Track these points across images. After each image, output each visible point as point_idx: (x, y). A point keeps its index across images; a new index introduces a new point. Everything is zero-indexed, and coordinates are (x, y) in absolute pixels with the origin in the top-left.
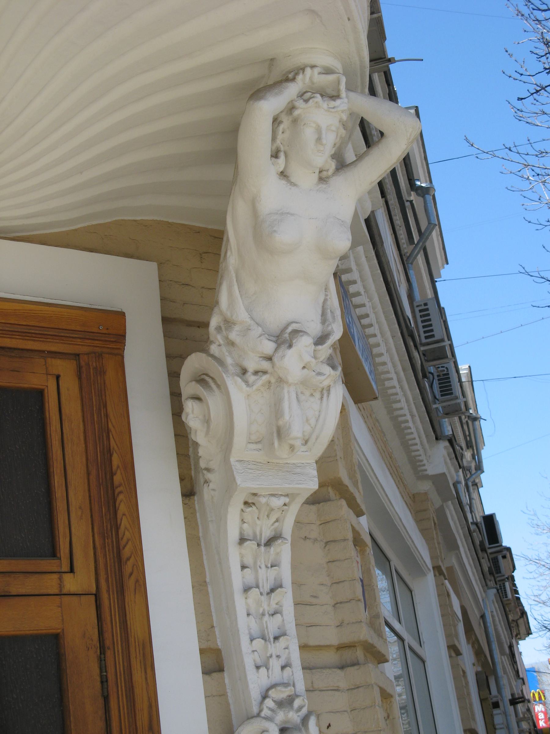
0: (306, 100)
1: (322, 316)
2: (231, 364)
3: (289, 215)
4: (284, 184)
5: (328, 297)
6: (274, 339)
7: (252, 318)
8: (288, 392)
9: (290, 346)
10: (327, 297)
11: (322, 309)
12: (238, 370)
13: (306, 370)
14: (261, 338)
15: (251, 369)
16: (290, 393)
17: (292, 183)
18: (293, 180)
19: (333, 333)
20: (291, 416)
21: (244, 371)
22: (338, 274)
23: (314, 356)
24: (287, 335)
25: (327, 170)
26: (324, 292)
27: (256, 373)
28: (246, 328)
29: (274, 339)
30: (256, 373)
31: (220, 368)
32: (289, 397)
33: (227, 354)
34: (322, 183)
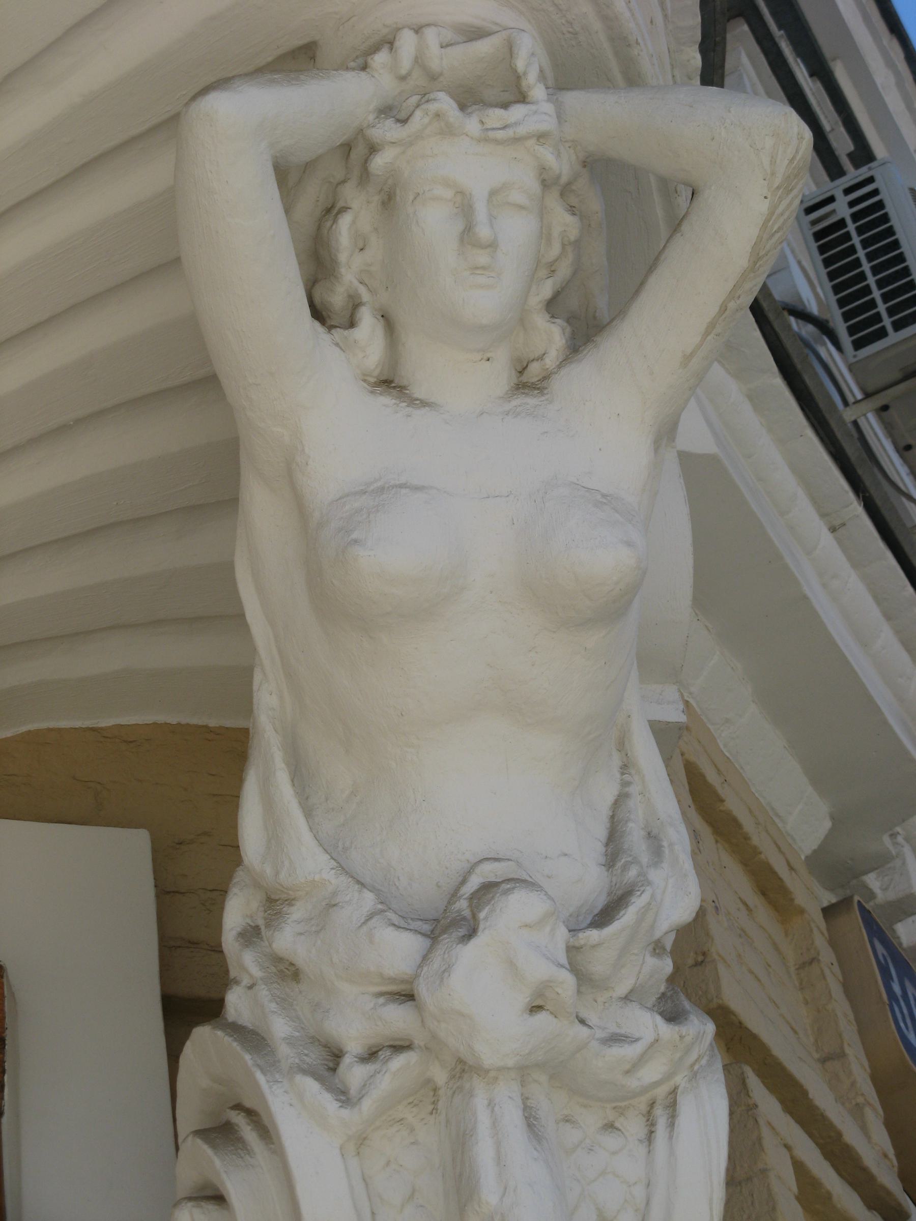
0: (405, 120)
1: (607, 845)
2: (284, 1039)
3: (404, 491)
4: (386, 406)
5: (632, 790)
6: (426, 928)
7: (343, 869)
8: (489, 1104)
9: (472, 933)
10: (627, 789)
11: (608, 825)
12: (314, 1057)
13: (542, 1018)
14: (373, 922)
15: (353, 1047)
16: (496, 1108)
17: (417, 400)
18: (419, 392)
19: (642, 889)
20: (506, 1188)
21: (335, 1055)
22: (856, 898)
23: (570, 964)
24: (462, 905)
25: (541, 358)
26: (618, 775)
27: (371, 1055)
28: (324, 904)
29: (426, 928)
30: (371, 1055)
31: (247, 1057)
32: (495, 1124)
33: (273, 1006)
34: (523, 393)
